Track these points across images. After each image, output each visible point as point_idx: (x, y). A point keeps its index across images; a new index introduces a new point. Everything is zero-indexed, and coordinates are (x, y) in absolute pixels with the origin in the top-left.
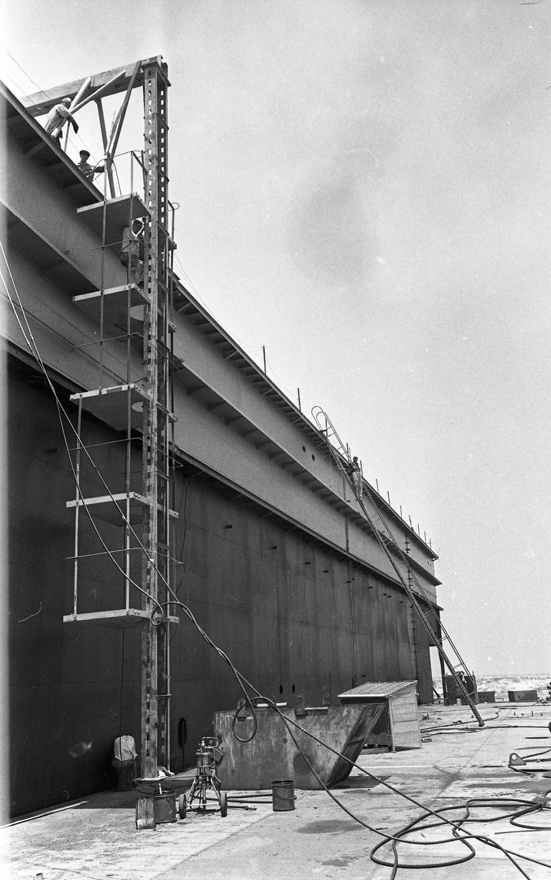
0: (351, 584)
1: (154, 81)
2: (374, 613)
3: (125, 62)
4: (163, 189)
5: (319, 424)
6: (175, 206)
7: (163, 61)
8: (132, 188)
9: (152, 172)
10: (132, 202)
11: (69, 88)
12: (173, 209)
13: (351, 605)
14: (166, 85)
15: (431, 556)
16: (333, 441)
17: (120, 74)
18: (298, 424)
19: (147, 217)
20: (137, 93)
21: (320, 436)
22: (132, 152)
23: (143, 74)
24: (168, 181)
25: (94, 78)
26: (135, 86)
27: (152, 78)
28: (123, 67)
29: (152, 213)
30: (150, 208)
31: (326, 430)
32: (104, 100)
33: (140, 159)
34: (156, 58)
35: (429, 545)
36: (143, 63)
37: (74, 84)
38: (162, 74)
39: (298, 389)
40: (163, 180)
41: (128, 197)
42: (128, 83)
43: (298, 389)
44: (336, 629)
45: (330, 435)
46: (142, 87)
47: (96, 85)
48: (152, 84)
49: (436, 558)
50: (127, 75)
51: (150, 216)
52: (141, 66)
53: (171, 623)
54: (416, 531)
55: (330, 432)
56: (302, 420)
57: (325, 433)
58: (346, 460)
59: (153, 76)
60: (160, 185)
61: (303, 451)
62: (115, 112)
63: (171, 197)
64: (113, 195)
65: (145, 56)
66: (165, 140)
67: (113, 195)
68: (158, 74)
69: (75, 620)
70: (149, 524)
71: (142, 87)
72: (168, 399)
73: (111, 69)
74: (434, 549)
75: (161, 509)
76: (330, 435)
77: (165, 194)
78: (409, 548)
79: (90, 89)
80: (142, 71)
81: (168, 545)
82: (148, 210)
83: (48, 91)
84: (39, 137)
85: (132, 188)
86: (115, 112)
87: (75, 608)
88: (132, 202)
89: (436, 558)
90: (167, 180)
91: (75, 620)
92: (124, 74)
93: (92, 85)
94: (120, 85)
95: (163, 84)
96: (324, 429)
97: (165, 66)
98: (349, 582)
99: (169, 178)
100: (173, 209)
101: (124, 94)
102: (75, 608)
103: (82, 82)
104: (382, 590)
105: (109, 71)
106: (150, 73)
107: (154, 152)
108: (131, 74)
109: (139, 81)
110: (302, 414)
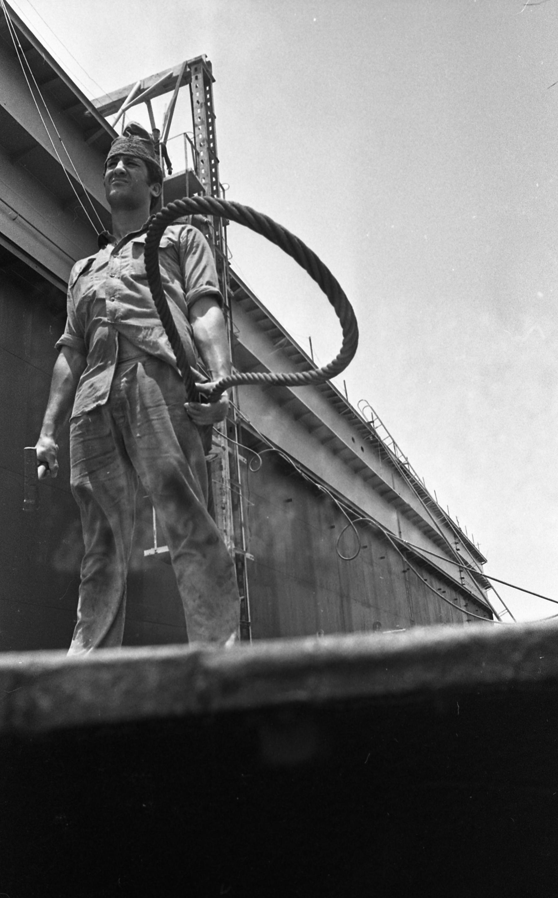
0: (407, 573)
1: (200, 76)
2: (431, 607)
3: (173, 65)
4: (213, 170)
5: (367, 416)
6: (225, 187)
7: (207, 60)
8: (187, 165)
9: (204, 153)
10: (187, 178)
11: (120, 93)
12: (224, 190)
13: (409, 595)
14: (211, 81)
15: (481, 559)
16: (381, 433)
17: (169, 74)
18: (346, 415)
19: (202, 192)
20: (184, 91)
21: (368, 428)
22: (185, 134)
23: (190, 72)
24: (218, 162)
25: (144, 81)
26: (182, 84)
27: (198, 73)
28: (170, 69)
29: (206, 188)
30: (205, 184)
31: (373, 422)
32: (153, 101)
33: (193, 140)
34: (201, 56)
35: (477, 547)
36: (188, 62)
37: (125, 89)
38: (207, 71)
39: (344, 381)
40: (213, 162)
41: (184, 172)
42: (176, 81)
43: (344, 381)
44: (396, 614)
45: (377, 427)
46: (188, 85)
47: (145, 87)
48: (198, 82)
49: (485, 561)
50: (174, 75)
51: (204, 191)
52: (188, 65)
53: (248, 559)
54: (464, 531)
55: (377, 423)
56: (350, 410)
57: (372, 424)
58: (392, 453)
59: (198, 72)
60: (212, 166)
61: (352, 442)
62: (166, 104)
63: (221, 180)
64: (170, 173)
65: (191, 57)
66: (213, 128)
67: (170, 173)
68: (203, 70)
69: (156, 553)
70: (221, 462)
71: (188, 85)
72: (206, 469)
73: (158, 72)
74: (483, 551)
75: (231, 452)
76: (377, 427)
77: (216, 175)
78: (458, 548)
79: (140, 90)
80: (188, 70)
81: (240, 483)
82: (202, 185)
83: (101, 98)
84: (100, 124)
85: (187, 165)
86: (166, 104)
87: (155, 542)
88: (187, 178)
89: (485, 561)
90: (217, 161)
91: (156, 553)
92: (171, 74)
93: (142, 88)
94: (168, 84)
95: (208, 80)
96: (370, 420)
97: (209, 64)
98: (404, 572)
99: (219, 159)
100: (224, 190)
101: (171, 94)
102: (155, 542)
103: (132, 86)
104: (436, 585)
105: (158, 74)
106: (196, 70)
107: (204, 136)
108: (178, 73)
109: (186, 79)
110: (350, 404)
